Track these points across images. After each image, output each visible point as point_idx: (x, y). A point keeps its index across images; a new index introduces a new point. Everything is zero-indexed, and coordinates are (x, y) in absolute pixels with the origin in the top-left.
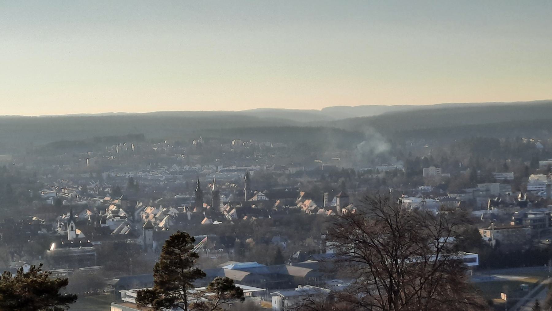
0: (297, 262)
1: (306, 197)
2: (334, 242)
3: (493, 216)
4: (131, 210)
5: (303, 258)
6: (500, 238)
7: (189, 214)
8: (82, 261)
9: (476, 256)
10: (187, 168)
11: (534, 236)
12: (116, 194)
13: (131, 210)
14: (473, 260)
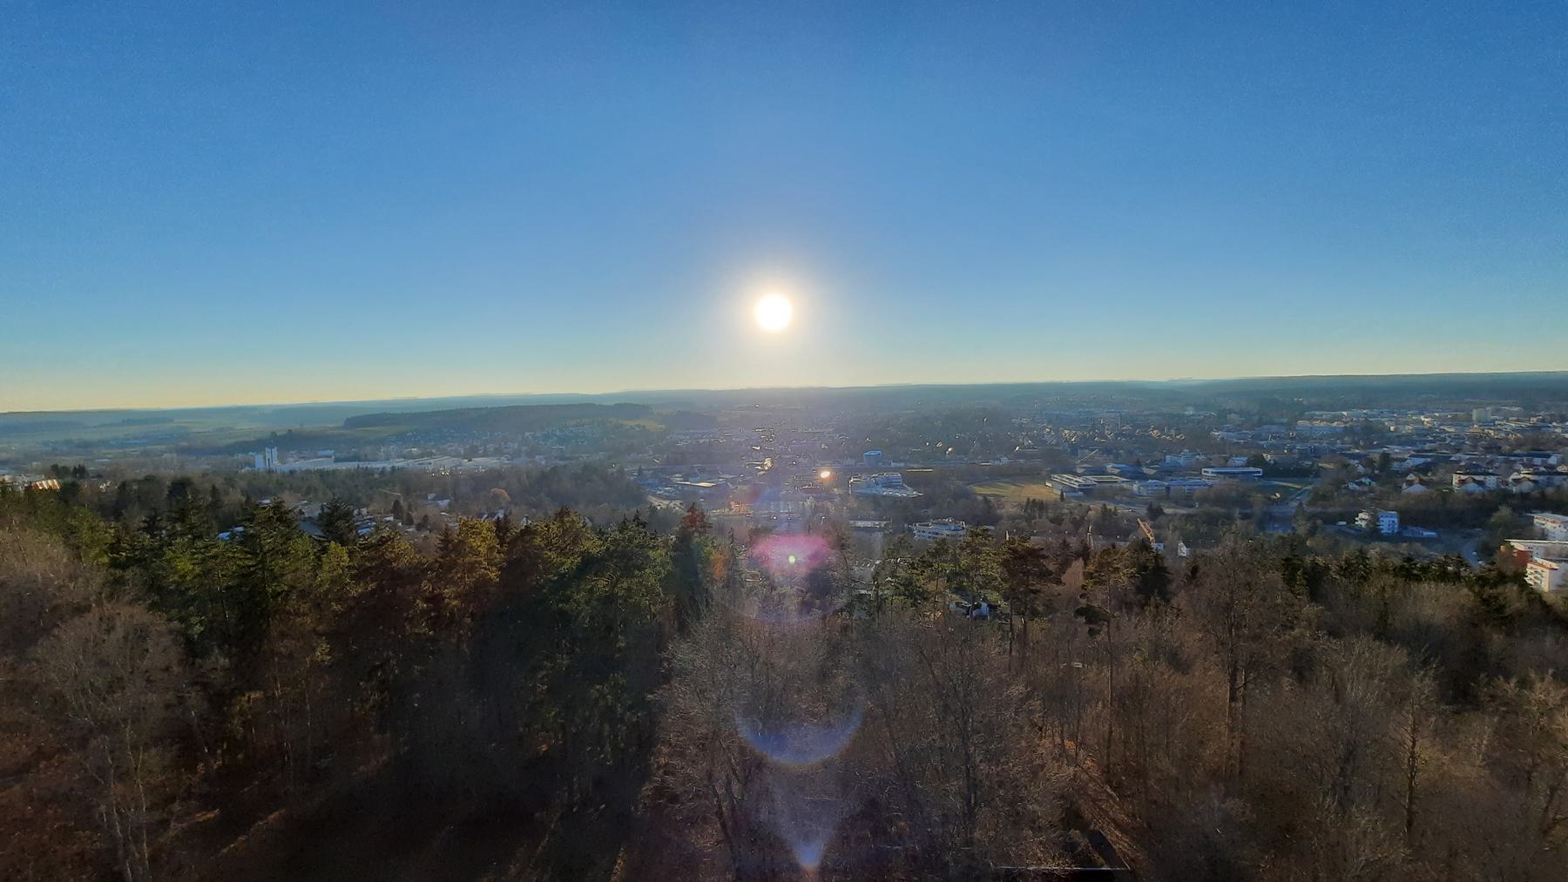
0: (1148, 466)
1: (1154, 429)
2: (104, 443)
3: (1272, 445)
4: (1057, 431)
5: (1152, 463)
6: (1277, 459)
7: (1088, 435)
8: (1032, 456)
9: (1261, 470)
10: (1087, 410)
11: (1299, 459)
12: (1050, 422)
13: (1057, 431)
14: (1259, 472)
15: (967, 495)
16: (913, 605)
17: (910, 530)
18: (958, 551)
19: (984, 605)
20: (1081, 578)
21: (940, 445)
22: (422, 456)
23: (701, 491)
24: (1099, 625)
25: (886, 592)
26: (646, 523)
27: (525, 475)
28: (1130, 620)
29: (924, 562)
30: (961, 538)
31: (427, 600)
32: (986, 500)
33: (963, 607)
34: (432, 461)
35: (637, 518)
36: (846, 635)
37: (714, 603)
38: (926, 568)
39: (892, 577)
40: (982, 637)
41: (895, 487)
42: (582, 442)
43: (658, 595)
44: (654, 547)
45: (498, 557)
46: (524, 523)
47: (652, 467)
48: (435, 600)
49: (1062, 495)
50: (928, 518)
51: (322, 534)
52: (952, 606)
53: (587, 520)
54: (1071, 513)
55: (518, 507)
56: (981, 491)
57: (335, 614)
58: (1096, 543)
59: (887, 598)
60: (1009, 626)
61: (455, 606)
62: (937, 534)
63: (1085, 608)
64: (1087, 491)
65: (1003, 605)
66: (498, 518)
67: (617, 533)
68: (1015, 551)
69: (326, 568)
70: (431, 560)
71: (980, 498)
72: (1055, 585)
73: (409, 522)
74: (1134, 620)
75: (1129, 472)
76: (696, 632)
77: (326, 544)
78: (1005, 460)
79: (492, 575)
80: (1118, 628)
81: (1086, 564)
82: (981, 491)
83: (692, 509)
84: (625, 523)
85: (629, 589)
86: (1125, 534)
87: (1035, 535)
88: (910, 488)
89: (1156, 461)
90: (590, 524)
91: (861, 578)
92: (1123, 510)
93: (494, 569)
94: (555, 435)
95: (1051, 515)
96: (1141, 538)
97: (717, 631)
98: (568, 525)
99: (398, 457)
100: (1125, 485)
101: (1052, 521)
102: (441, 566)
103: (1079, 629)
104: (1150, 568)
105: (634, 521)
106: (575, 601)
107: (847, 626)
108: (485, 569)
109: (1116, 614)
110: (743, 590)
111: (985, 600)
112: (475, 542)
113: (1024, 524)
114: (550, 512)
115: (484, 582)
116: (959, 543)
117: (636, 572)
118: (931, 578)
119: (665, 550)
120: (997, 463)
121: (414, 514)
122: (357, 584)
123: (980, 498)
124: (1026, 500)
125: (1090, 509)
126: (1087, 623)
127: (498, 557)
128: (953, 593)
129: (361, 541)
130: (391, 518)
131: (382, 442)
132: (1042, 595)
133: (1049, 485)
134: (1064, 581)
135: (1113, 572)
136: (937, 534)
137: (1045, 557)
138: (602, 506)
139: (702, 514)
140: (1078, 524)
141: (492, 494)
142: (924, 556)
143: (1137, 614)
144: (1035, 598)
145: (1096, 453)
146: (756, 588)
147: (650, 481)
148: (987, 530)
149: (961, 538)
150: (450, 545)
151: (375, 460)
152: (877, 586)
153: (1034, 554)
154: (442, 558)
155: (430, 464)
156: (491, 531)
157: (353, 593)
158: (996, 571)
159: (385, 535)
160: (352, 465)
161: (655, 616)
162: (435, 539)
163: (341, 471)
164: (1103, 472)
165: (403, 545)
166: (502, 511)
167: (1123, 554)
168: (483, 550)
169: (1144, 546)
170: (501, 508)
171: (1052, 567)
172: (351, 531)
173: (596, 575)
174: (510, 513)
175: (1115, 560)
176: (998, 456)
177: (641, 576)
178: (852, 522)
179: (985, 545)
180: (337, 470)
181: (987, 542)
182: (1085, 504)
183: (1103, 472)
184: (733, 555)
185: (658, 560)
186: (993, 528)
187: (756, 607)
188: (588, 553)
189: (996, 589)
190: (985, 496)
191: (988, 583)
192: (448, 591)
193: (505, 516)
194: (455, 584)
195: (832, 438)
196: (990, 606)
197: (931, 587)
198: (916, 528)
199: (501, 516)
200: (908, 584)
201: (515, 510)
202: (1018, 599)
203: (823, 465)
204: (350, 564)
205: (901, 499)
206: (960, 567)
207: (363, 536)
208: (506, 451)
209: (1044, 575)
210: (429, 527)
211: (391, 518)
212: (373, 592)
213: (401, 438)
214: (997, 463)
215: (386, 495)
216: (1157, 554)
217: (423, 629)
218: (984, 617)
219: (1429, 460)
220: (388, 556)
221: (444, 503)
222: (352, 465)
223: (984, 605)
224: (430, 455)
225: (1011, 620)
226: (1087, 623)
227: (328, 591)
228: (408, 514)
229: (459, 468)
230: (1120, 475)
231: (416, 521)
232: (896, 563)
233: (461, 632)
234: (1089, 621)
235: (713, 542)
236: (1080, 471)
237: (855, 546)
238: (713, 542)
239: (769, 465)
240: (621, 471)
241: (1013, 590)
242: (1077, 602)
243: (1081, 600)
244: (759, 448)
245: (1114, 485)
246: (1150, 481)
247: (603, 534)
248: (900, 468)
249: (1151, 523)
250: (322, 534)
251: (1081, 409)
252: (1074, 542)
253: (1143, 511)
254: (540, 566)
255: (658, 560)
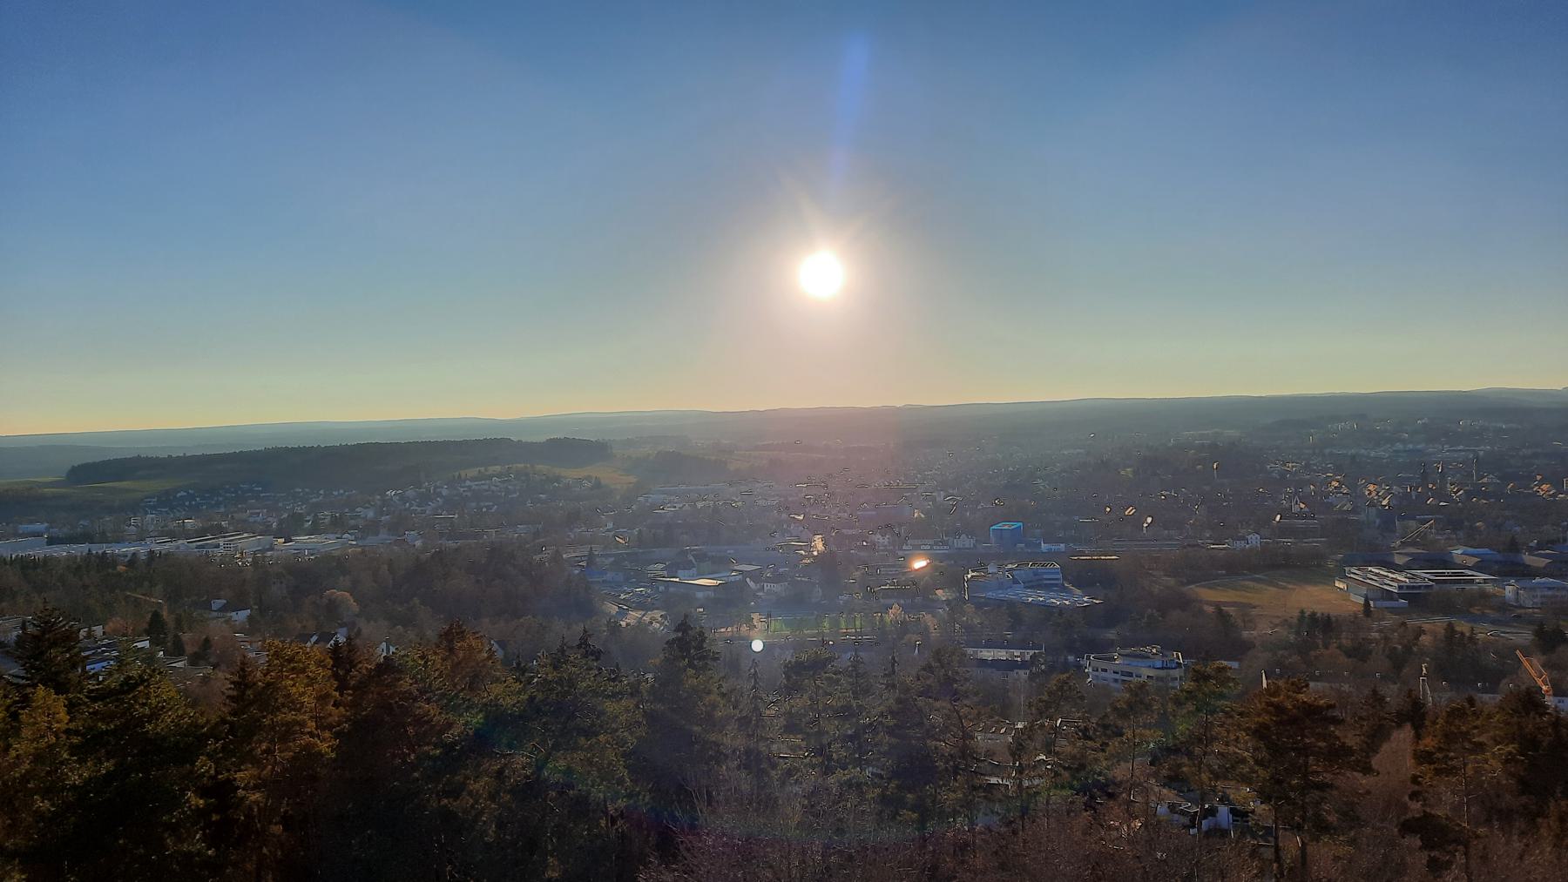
0: (1531, 550)
1: (1542, 482)
5: (1540, 547)
10: (1411, 446)
15: (1185, 603)
16: (1088, 806)
17: (1080, 667)
18: (1170, 707)
19: (1223, 810)
20: (1410, 762)
21: (1130, 511)
22: (201, 533)
23: (700, 595)
24: (1448, 852)
25: (1036, 782)
26: (600, 652)
27: (386, 567)
28: (1508, 843)
29: (1105, 727)
30: (1177, 684)
31: (203, 792)
32: (1221, 615)
33: (1183, 813)
34: (221, 542)
35: (583, 643)
36: (963, 862)
37: (721, 798)
38: (1109, 738)
39: (1049, 753)
40: (1221, 871)
41: (1048, 587)
42: (489, 508)
43: (621, 781)
44: (614, 695)
45: (335, 714)
46: (382, 651)
47: (615, 551)
48: (221, 792)
49: (1367, 604)
50: (1110, 645)
51: (22, 673)
52: (1162, 810)
53: (496, 647)
54: (1386, 639)
55: (372, 623)
56: (1209, 595)
57: (39, 815)
58: (1435, 696)
59: (1037, 793)
60: (1273, 850)
61: (257, 802)
62: (1130, 675)
63: (1419, 819)
64: (1416, 599)
65: (1258, 811)
66: (337, 643)
67: (549, 669)
68: (1279, 709)
69: (26, 733)
70: (214, 719)
71: (1210, 609)
72: (1358, 775)
73: (177, 650)
74: (1518, 845)
75: (1496, 562)
76: (688, 850)
77: (29, 690)
78: (1255, 540)
79: (324, 747)
80: (1484, 858)
81: (1418, 737)
82: (1209, 595)
83: (683, 627)
84: (563, 651)
85: (569, 771)
86: (1492, 678)
87: (1317, 679)
88: (1078, 592)
89: (1549, 542)
90: (500, 654)
91: (990, 754)
92: (1484, 633)
93: (327, 734)
94: (440, 495)
95: (1346, 642)
96: (1523, 687)
97: (727, 850)
98: (461, 655)
99: (162, 534)
100: (1489, 588)
101: (1349, 653)
102: (232, 731)
103: (1408, 859)
104: (1545, 744)
105: (579, 646)
106: (470, 793)
107: (966, 844)
108: (311, 734)
109: (1481, 831)
110: (773, 773)
111: (1224, 800)
112: (295, 687)
113: (1295, 658)
114: (429, 633)
115: (310, 756)
116: (1173, 692)
117: (582, 740)
118: (1119, 758)
119: (634, 701)
120: (1240, 545)
121: (186, 637)
122: (81, 761)
123: (1210, 609)
124: (1296, 613)
125: (1424, 632)
126: (1425, 847)
127: (335, 714)
128: (1164, 786)
129: (91, 685)
130: (146, 644)
131: (135, 507)
132: (1335, 793)
133: (1341, 586)
134: (1375, 766)
135: (1471, 752)
136: (1130, 675)
137: (1336, 721)
138: (521, 620)
139: (701, 634)
140: (1399, 661)
141: (325, 601)
142: (1106, 716)
143: (1523, 834)
144: (1323, 799)
145: (1431, 528)
146: (798, 770)
147: (609, 576)
148: (1224, 669)
149: (1177, 684)
150: (249, 692)
151: (119, 540)
152: (1020, 771)
153: (1315, 715)
154: (234, 714)
155: (218, 546)
156: (324, 667)
157: (74, 779)
158: (1245, 748)
159: (134, 673)
160: (79, 550)
161: (614, 821)
162: (222, 681)
163: (58, 560)
164: (1446, 563)
165: (166, 690)
166: (344, 630)
167: (1490, 716)
168: (308, 701)
169: (1530, 701)
170: (341, 626)
171: (1352, 740)
172: (74, 666)
173: (510, 746)
174: (359, 633)
175: (1476, 727)
176: (1242, 532)
177: (591, 748)
178: (970, 651)
179: (1222, 696)
180: (52, 558)
181: (1225, 691)
182: (1413, 622)
183: (1446, 563)
184: (756, 709)
185: (622, 718)
186: (1235, 665)
187: (798, 807)
188: (496, 705)
189: (1245, 779)
190: (1218, 605)
191: (1229, 769)
192: (243, 776)
193: (349, 638)
194: (256, 762)
195: (934, 500)
196: (1233, 811)
197: (1121, 772)
198: (1090, 664)
199: (342, 639)
200: (1079, 766)
201: (366, 628)
202: (1288, 798)
203: (917, 547)
204: (72, 726)
205: (1061, 610)
206: (1175, 737)
207: (96, 675)
208: (352, 522)
209: (1337, 755)
210: (212, 660)
211: (146, 644)
212: (110, 776)
213: (166, 501)
214: (1240, 545)
215: (137, 603)
216: (1558, 718)
217: (196, 843)
218: (1224, 833)
219: (1306, 540)
220: (139, 711)
221: (242, 616)
222: (79, 550)
223: (1223, 810)
224: (219, 531)
225: (1276, 838)
226: (1425, 847)
227: (25, 778)
228: (176, 636)
229: (269, 553)
230: (1478, 568)
231: (189, 649)
232: (1055, 728)
233: (265, 850)
234: (1427, 845)
235: (720, 686)
236: (1400, 560)
237: (976, 694)
238: (720, 686)
239: (820, 546)
240: (557, 557)
241: (1279, 782)
242: (1405, 808)
243: (1410, 803)
244: (801, 518)
245: (1468, 587)
246: (1538, 580)
247: (524, 671)
248: (1058, 553)
249: (1543, 658)
250: (22, 673)
251: (1399, 446)
252: (1392, 694)
253: (1524, 636)
254: (410, 730)
255: (622, 718)
